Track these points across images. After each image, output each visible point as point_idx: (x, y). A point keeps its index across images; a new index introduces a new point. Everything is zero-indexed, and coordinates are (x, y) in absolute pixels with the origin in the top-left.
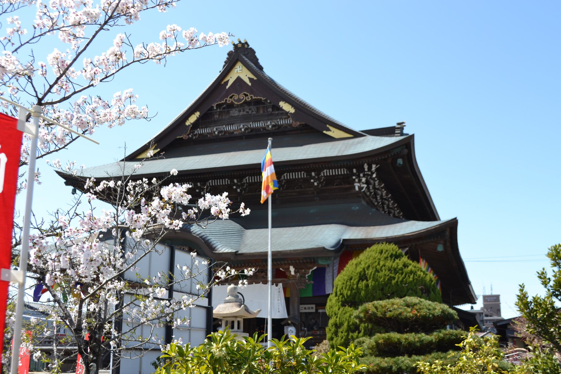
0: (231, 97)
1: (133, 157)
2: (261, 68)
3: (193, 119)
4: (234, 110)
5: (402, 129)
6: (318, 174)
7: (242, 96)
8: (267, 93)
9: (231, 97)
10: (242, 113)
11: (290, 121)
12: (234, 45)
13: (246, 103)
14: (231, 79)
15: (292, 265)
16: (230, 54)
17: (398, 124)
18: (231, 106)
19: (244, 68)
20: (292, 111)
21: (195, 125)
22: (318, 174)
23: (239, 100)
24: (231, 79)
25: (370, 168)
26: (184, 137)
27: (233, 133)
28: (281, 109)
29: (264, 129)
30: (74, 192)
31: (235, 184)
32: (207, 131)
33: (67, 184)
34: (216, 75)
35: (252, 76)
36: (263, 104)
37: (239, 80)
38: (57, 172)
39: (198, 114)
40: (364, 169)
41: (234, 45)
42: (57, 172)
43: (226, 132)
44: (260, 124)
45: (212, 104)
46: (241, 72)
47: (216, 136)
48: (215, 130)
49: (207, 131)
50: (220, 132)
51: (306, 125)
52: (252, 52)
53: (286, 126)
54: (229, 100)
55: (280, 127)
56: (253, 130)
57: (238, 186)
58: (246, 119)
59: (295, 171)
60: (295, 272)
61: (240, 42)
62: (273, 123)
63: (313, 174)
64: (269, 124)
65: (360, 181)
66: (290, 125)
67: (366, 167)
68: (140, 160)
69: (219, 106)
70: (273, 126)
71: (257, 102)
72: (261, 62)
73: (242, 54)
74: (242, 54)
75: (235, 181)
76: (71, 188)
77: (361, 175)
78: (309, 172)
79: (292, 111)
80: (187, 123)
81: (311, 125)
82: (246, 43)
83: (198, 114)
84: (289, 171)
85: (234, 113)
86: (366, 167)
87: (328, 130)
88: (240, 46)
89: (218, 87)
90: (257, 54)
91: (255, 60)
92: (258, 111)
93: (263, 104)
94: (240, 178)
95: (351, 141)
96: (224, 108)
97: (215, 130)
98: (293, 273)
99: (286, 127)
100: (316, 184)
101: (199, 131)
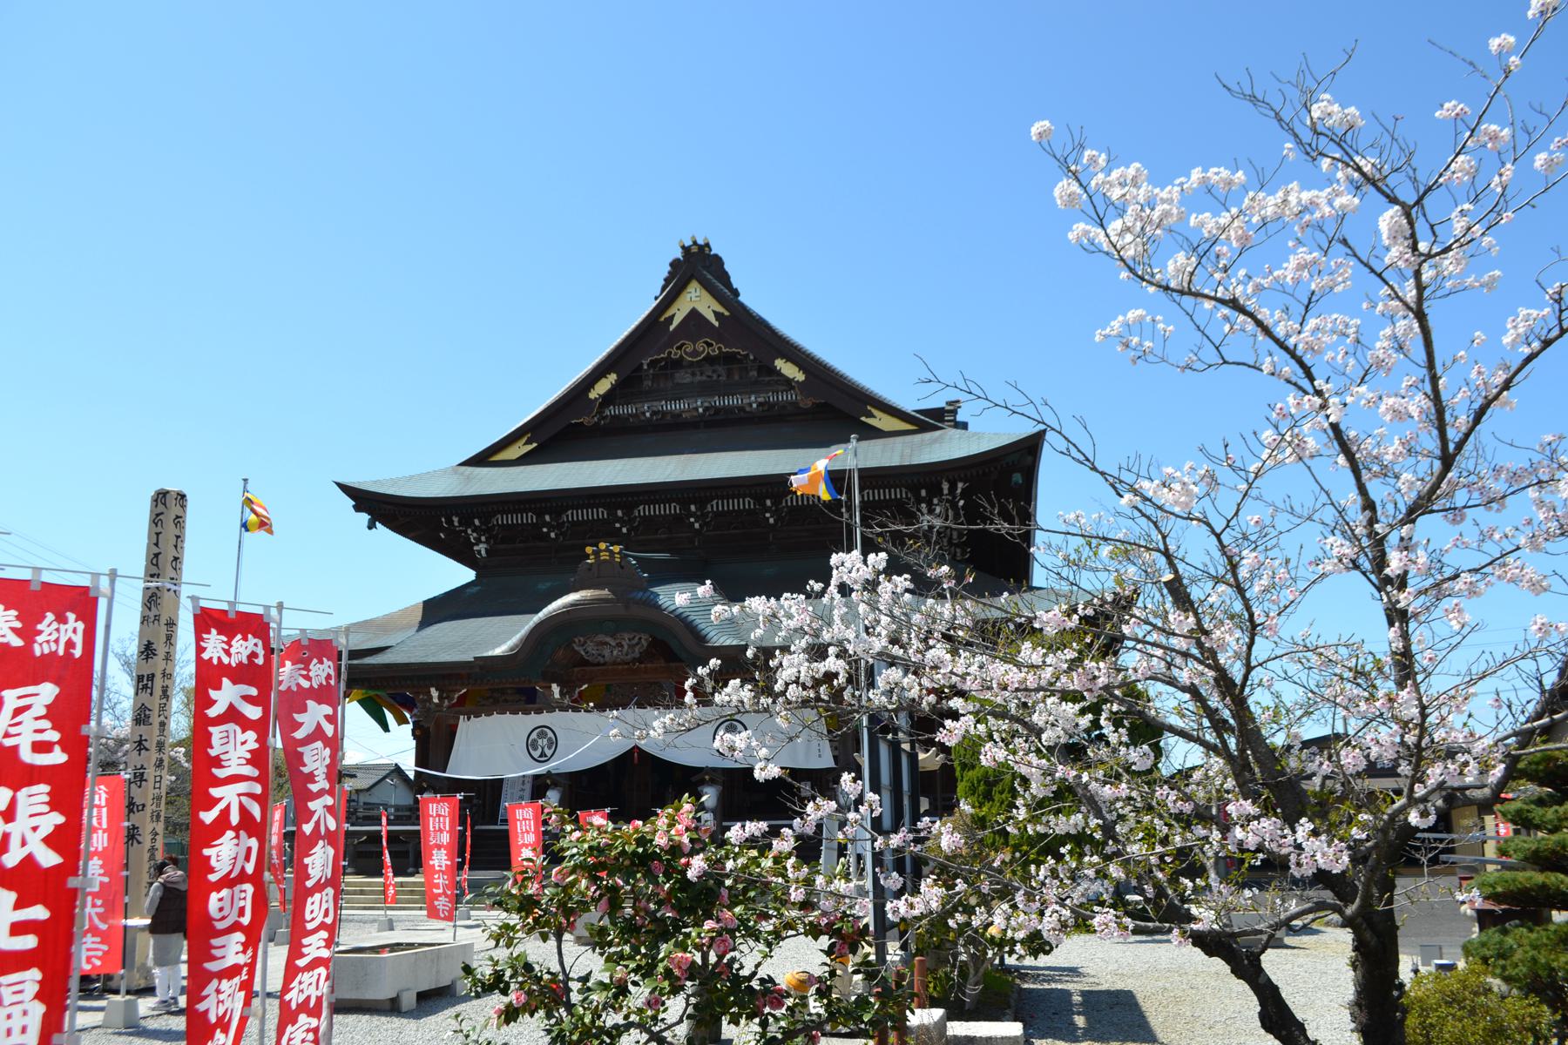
0: (679, 348)
1: (482, 460)
2: (736, 293)
3: (603, 386)
4: (682, 372)
5: (954, 412)
6: (702, 506)
7: (700, 346)
8: (749, 342)
9: (679, 348)
10: (698, 378)
11: (789, 397)
12: (683, 247)
13: (709, 360)
14: (680, 311)
15: (65, 882)
16: (675, 264)
17: (949, 403)
18: (678, 364)
19: (704, 293)
20: (800, 377)
21: (608, 399)
22: (702, 506)
23: (695, 353)
24: (680, 311)
25: (450, 522)
26: (585, 420)
27: (680, 415)
28: (779, 373)
29: (741, 409)
30: (371, 526)
31: (546, 524)
32: (630, 409)
33: (358, 508)
34: (645, 307)
35: (720, 309)
36: (740, 361)
37: (694, 314)
38: (339, 485)
39: (613, 377)
40: (942, 489)
41: (683, 247)
42: (339, 485)
43: (664, 413)
44: (733, 401)
45: (642, 358)
46: (696, 299)
47: (650, 420)
48: (647, 409)
49: (630, 409)
50: (654, 413)
51: (825, 405)
52: (718, 260)
53: (784, 406)
54: (675, 353)
55: (771, 406)
56: (718, 410)
57: (551, 527)
58: (706, 389)
59: (516, 512)
60: (440, 697)
61: (695, 243)
62: (761, 400)
63: (693, 508)
64: (753, 401)
65: (931, 512)
66: (794, 404)
67: (945, 486)
68: (1460, 446)
69: (652, 364)
70: (760, 404)
71: (728, 359)
72: (736, 282)
73: (698, 265)
74: (698, 265)
75: (547, 518)
76: (364, 517)
77: (935, 501)
78: (684, 504)
79: (800, 377)
80: (593, 395)
81: (836, 407)
82: (707, 245)
83: (613, 377)
84: (502, 512)
85: (684, 377)
86: (945, 486)
87: (871, 415)
88: (695, 249)
89: (652, 326)
90: (728, 267)
91: (725, 278)
92: (729, 374)
93: (740, 361)
94: (702, 503)
95: (918, 438)
96: (661, 368)
97: (647, 409)
98: (436, 700)
99: (784, 407)
100: (697, 526)
101: (611, 411)
